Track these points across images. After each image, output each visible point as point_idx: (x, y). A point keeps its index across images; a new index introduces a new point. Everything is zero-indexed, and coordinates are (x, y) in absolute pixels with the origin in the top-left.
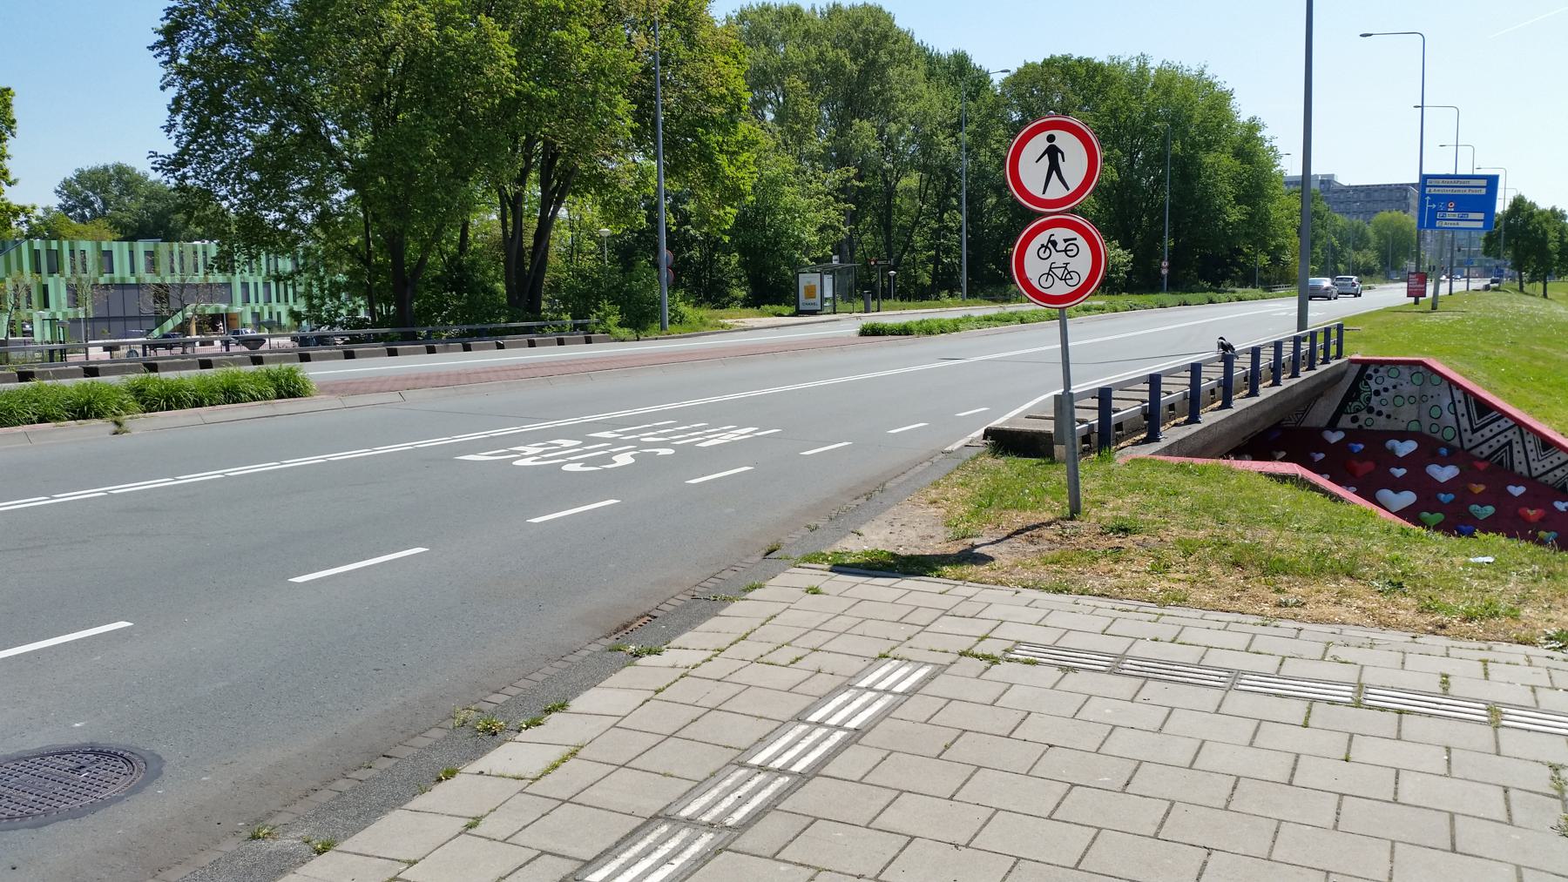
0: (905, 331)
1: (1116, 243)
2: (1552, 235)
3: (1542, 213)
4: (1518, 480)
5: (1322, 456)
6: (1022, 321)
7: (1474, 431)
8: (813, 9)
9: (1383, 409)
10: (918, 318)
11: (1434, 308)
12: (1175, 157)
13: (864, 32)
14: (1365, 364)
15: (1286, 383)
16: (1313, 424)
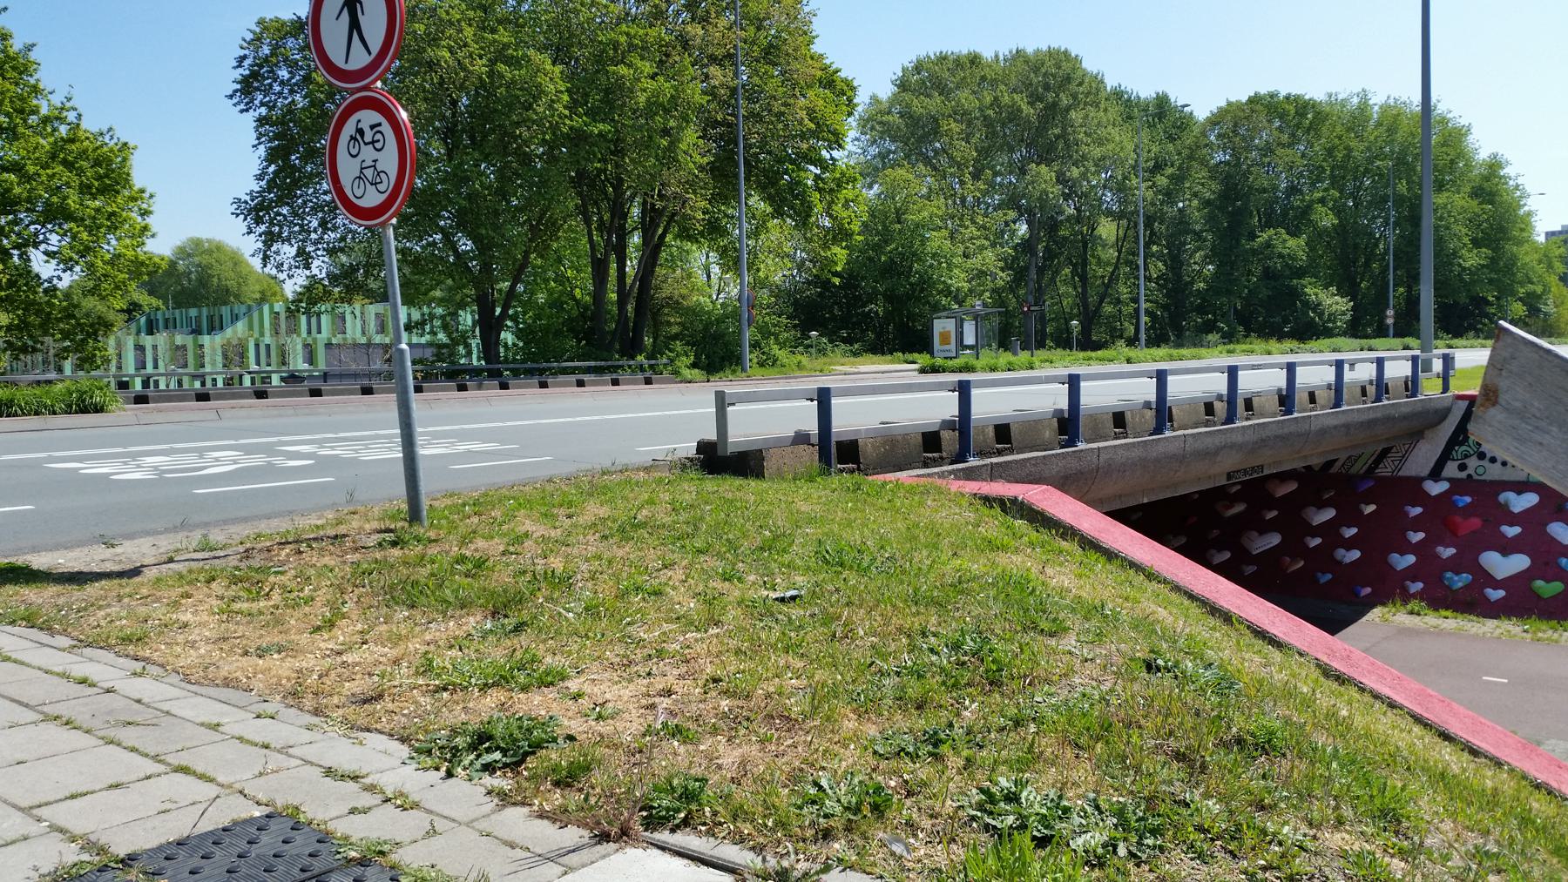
1: (1333, 289)
5: (1419, 510)
8: (997, 56)
13: (1045, 74)
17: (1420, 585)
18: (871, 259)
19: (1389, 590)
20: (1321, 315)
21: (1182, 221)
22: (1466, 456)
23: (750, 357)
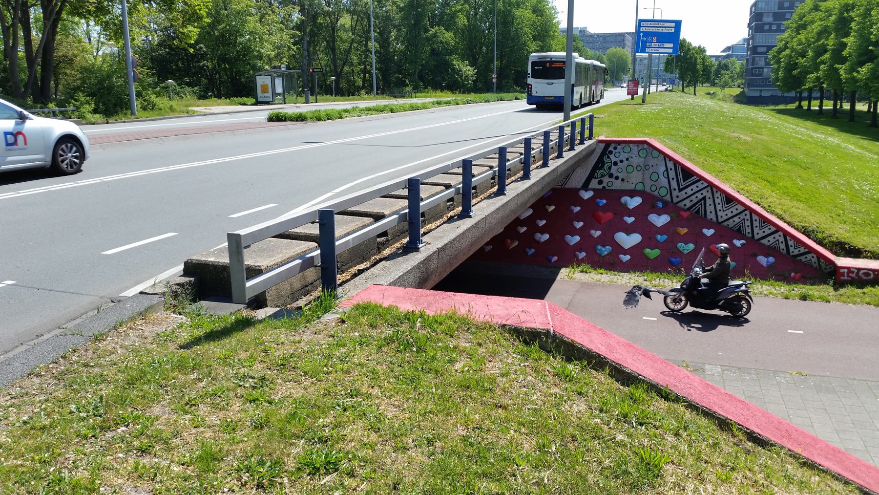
0: (301, 118)
2: (699, 61)
3: (694, 48)
4: (710, 225)
5: (578, 208)
6: (392, 111)
7: (680, 190)
9: (620, 175)
10: (375, 105)
11: (643, 101)
12: (499, 11)
14: (608, 143)
15: (554, 164)
16: (573, 186)
17: (584, 254)
18: (209, 33)
19: (569, 259)
20: (461, 77)
21: (387, 18)
22: (603, 176)
23: (137, 103)
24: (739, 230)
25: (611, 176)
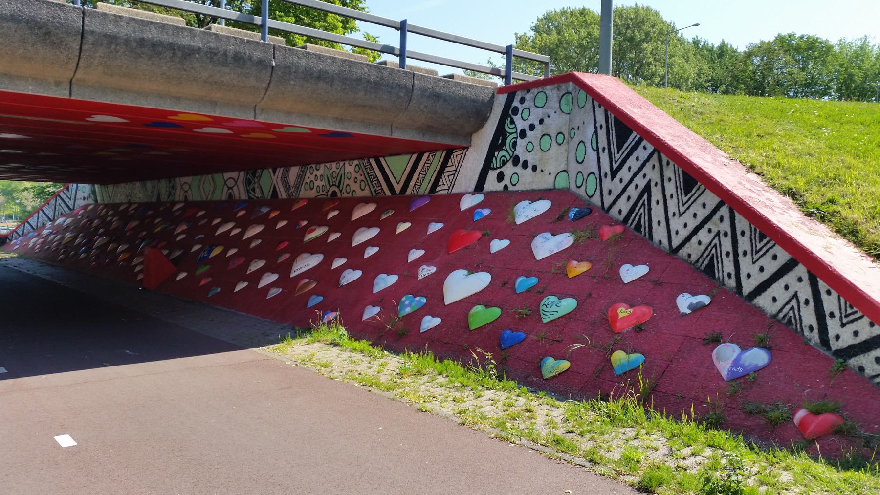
24: (710, 269)
25: (516, 161)
